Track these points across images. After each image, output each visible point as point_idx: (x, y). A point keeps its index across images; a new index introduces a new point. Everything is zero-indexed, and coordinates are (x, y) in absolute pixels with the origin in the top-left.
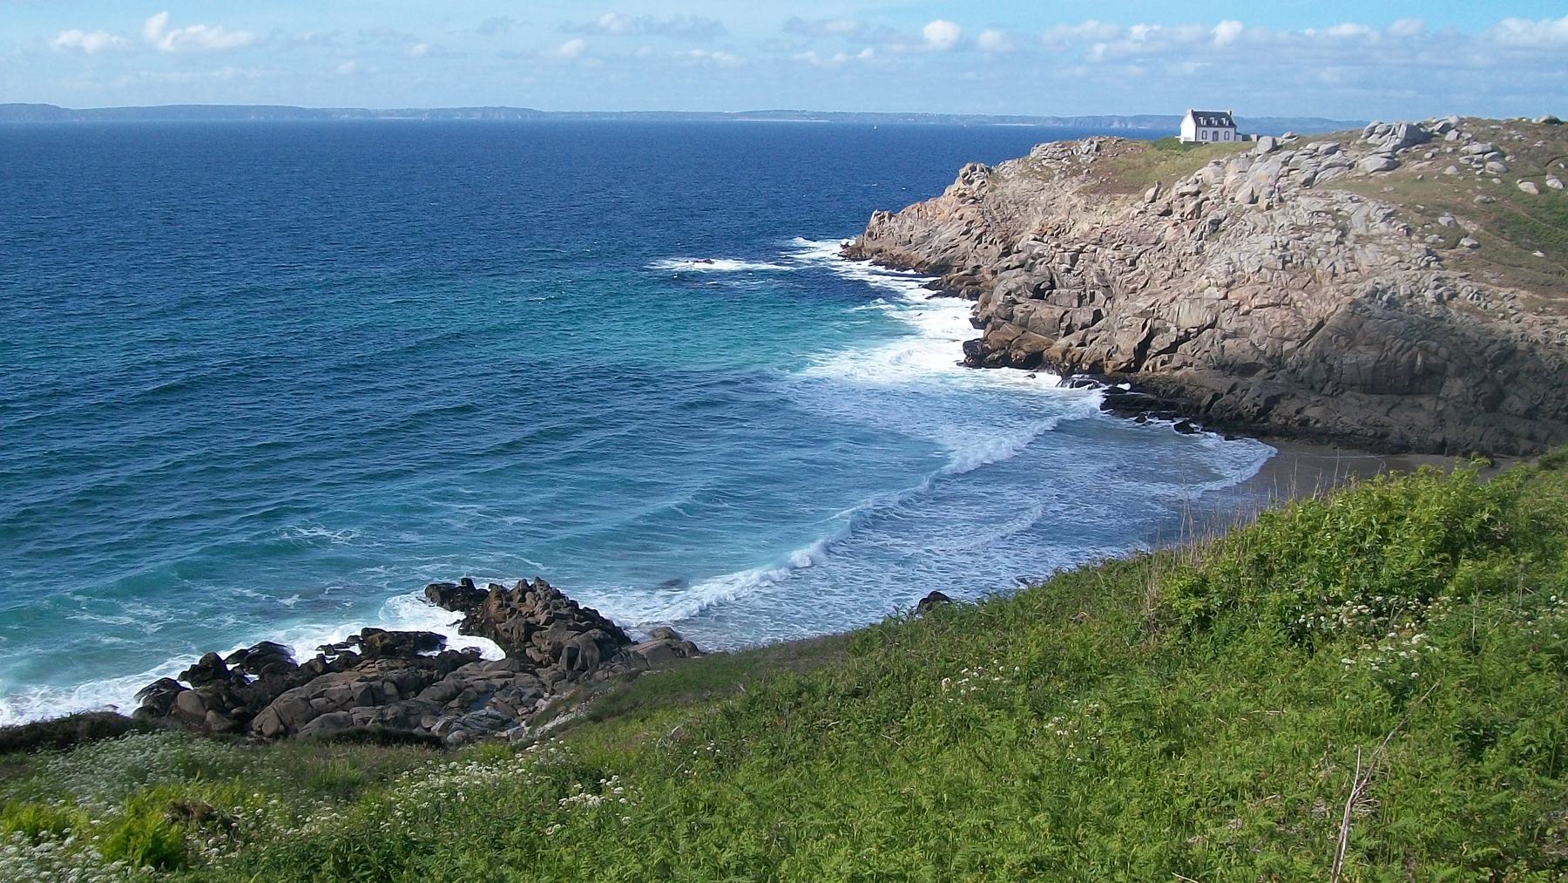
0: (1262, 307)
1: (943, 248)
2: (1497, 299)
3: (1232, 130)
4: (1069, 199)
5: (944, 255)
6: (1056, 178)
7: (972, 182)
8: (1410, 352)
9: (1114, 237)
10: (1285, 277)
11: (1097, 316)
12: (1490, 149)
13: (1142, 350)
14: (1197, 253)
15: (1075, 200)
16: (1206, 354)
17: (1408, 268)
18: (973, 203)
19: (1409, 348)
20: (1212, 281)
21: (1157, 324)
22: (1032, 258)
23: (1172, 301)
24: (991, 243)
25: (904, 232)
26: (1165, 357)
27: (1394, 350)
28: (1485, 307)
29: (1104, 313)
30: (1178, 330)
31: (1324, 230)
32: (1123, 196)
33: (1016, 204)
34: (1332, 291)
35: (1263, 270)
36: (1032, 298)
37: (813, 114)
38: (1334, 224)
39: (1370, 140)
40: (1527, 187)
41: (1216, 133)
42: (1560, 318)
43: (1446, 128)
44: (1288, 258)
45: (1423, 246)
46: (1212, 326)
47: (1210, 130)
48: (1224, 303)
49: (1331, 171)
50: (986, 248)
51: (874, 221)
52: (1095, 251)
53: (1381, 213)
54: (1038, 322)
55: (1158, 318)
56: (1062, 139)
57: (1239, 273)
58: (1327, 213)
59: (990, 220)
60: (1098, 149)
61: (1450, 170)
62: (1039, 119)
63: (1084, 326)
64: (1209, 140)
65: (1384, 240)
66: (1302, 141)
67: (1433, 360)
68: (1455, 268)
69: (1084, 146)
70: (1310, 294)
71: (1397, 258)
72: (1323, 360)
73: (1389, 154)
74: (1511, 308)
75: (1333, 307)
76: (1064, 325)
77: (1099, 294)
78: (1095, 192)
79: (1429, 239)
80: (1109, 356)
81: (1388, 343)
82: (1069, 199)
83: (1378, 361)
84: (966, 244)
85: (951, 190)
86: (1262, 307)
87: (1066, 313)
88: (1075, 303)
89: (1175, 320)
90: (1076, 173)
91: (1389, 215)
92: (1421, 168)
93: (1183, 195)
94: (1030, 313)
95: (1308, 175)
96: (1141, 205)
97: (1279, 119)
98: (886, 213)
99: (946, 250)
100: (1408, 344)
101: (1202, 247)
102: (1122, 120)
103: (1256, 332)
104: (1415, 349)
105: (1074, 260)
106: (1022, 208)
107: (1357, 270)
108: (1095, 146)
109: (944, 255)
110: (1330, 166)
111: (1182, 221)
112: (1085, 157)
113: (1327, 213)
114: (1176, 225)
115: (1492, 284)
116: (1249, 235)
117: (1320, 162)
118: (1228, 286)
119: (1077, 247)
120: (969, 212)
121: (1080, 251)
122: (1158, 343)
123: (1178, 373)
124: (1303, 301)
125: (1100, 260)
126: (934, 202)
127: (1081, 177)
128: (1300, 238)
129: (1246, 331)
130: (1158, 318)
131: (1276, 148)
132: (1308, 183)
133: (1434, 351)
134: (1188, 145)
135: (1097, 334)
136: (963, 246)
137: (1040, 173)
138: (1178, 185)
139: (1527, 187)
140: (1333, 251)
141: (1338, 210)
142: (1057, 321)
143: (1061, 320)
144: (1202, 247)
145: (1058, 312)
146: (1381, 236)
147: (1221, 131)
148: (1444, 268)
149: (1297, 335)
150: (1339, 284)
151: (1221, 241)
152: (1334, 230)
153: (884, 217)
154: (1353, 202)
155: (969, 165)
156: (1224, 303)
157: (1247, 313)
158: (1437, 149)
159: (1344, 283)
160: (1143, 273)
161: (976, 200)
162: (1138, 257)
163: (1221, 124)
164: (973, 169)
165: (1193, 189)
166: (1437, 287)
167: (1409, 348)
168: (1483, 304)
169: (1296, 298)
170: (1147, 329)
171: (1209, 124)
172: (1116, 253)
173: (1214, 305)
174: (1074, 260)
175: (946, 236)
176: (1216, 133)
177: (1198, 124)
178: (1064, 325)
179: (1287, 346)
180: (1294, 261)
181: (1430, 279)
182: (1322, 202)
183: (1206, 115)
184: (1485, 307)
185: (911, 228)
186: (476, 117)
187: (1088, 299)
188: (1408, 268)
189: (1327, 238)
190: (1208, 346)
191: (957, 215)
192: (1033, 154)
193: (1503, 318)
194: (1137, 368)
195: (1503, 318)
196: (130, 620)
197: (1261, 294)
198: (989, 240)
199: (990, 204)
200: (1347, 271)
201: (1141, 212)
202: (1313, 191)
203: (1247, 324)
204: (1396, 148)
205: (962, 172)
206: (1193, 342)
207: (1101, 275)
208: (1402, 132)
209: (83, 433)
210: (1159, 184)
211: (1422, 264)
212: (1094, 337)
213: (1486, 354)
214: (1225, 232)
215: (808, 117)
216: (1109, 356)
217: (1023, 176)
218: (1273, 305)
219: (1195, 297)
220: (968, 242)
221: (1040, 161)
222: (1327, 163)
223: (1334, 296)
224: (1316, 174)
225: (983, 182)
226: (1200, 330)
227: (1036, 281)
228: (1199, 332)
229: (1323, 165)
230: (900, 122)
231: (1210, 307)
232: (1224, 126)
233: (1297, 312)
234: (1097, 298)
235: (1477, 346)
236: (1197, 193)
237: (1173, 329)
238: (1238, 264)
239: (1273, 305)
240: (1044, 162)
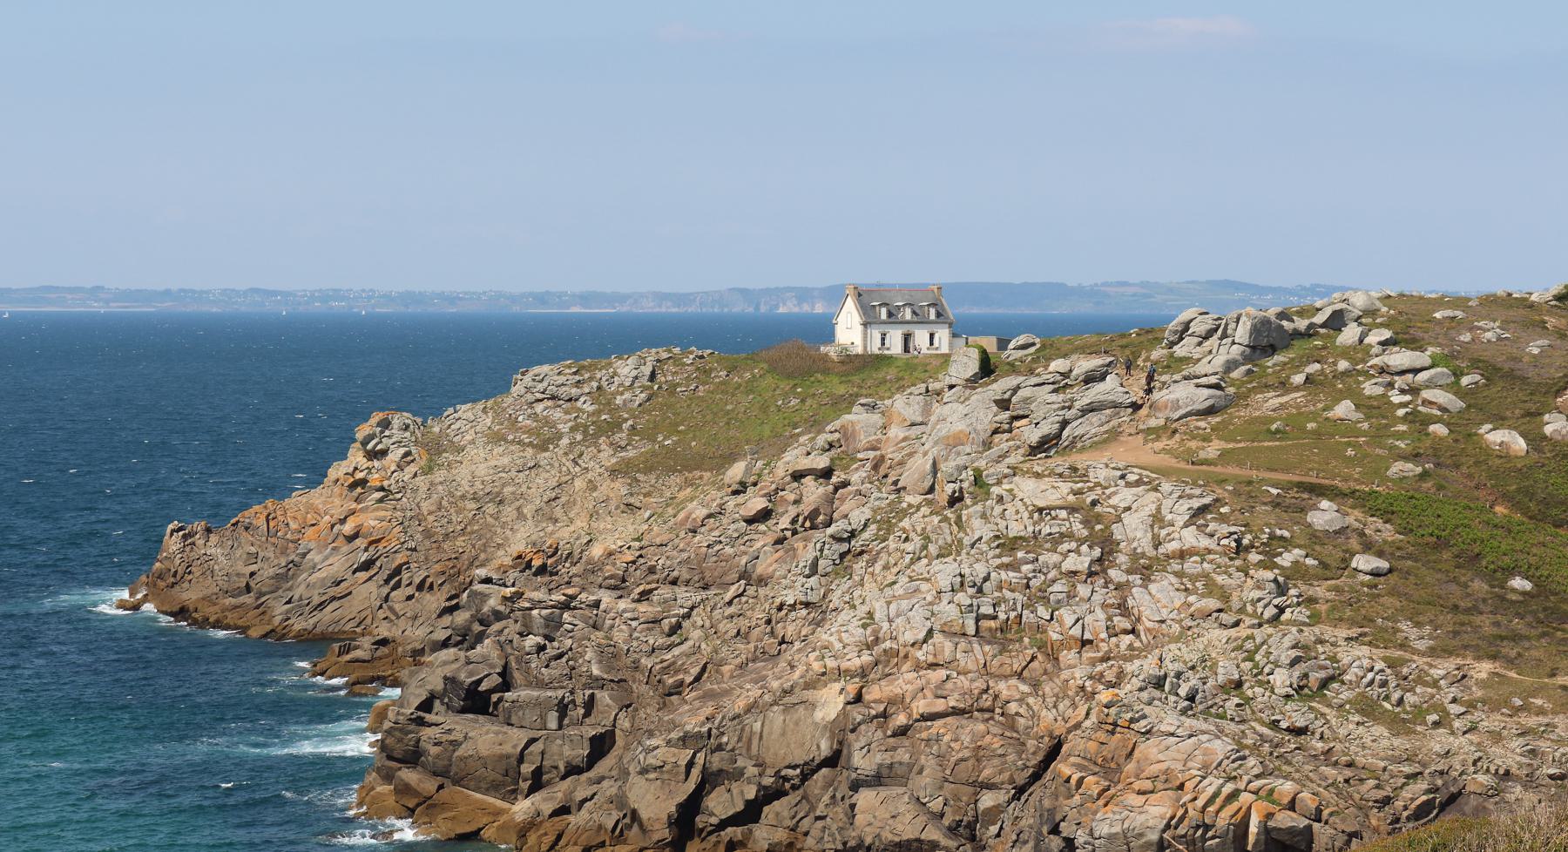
1: (316, 600)
2: (1426, 684)
5: (318, 616)
6: (565, 441)
8: (1235, 806)
9: (652, 570)
11: (601, 745)
12: (1428, 362)
16: (820, 824)
17: (1237, 624)
18: (381, 500)
19: (1233, 796)
21: (717, 761)
22: (481, 622)
27: (1200, 803)
28: (1400, 702)
31: (1065, 547)
34: (1079, 674)
35: (938, 638)
36: (463, 711)
38: (1085, 533)
39: (1179, 351)
40: (1507, 439)
42: (1559, 720)
43: (1337, 321)
45: (1269, 575)
46: (832, 761)
49: (1094, 418)
50: (410, 598)
51: (173, 544)
53: (1184, 506)
56: (576, 355)
58: (1072, 510)
59: (418, 537)
61: (1344, 409)
62: (622, 298)
63: (573, 770)
65: (1191, 566)
66: (1048, 351)
67: (1285, 820)
68: (1337, 622)
69: (625, 369)
70: (1036, 685)
71: (1213, 603)
72: (1055, 830)
73: (1213, 380)
74: (1454, 701)
75: (1082, 710)
76: (527, 769)
78: (648, 470)
79: (1286, 559)
81: (1189, 785)
83: (1168, 826)
85: (338, 471)
87: (532, 741)
88: (553, 723)
91: (1203, 510)
92: (1282, 406)
93: (798, 476)
94: (455, 744)
95: (1048, 428)
96: (715, 497)
97: (1144, 285)
98: (199, 526)
100: (1229, 788)
103: (920, 772)
104: (1246, 798)
107: (1133, 631)
108: (647, 370)
110: (1091, 409)
111: (795, 532)
113: (1072, 510)
114: (780, 541)
115: (1415, 652)
116: (912, 562)
117: (1072, 400)
118: (863, 673)
122: (720, 804)
124: (1021, 701)
125: (608, 622)
129: (899, 770)
130: (720, 748)
131: (987, 369)
132: (1044, 446)
133: (1286, 801)
135: (594, 788)
137: (529, 431)
138: (788, 456)
139: (1507, 439)
140: (1083, 590)
141: (1094, 503)
142: (514, 761)
145: (517, 737)
146: (1182, 555)
148: (1315, 619)
149: (1006, 775)
150: (1093, 663)
151: (857, 578)
152: (1084, 548)
154: (1128, 485)
155: (377, 417)
157: (903, 732)
158: (1317, 366)
159: (1106, 659)
160: (697, 650)
162: (688, 616)
164: (385, 424)
165: (822, 462)
166: (1294, 662)
167: (1233, 796)
168: (1396, 696)
169: (1005, 694)
172: (643, 607)
179: (987, 800)
180: (1002, 616)
181: (1282, 646)
182: (1065, 487)
184: (1400, 702)
188: (1237, 624)
189: (1071, 563)
190: (821, 806)
192: (517, 389)
193: (1436, 724)
195: (1436, 724)
200: (1113, 632)
201: (710, 516)
202: (1051, 463)
203: (903, 755)
204: (1230, 366)
205: (362, 431)
206: (792, 798)
207: (609, 655)
208: (1242, 333)
211: (1267, 615)
212: (589, 793)
213: (1399, 804)
214: (866, 557)
217: (497, 438)
218: (956, 712)
220: (372, 586)
222: (1086, 401)
223: (1083, 688)
224: (1064, 424)
225: (408, 454)
226: (808, 771)
227: (471, 674)
228: (805, 777)
229: (1078, 405)
233: (1010, 722)
234: (599, 706)
235: (1378, 787)
236: (826, 474)
238: (885, 625)
240: (539, 408)
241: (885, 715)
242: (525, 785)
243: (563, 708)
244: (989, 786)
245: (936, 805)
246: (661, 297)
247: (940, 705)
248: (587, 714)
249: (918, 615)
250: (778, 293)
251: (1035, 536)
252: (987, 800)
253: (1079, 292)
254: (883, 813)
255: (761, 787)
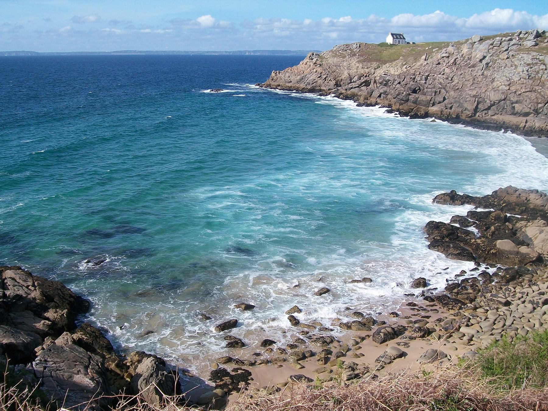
0: (526, 92)
3: (404, 40)
4: (355, 65)
5: (313, 85)
7: (312, 59)
10: (531, 82)
13: (476, 110)
14: (482, 75)
15: (357, 65)
20: (503, 83)
23: (486, 91)
24: (330, 80)
25: (286, 78)
26: (486, 111)
29: (446, 97)
30: (491, 101)
32: (375, 63)
33: (335, 66)
37: (139, 52)
41: (399, 41)
44: (530, 75)
46: (504, 100)
47: (397, 40)
48: (509, 91)
51: (273, 74)
52: (434, 76)
54: (421, 101)
55: (480, 98)
57: (512, 80)
60: (360, 47)
62: (220, 52)
64: (397, 43)
76: (432, 102)
77: (443, 91)
78: (364, 62)
80: (462, 112)
82: (355, 65)
84: (320, 81)
86: (526, 92)
88: (433, 94)
89: (488, 98)
90: (355, 55)
93: (443, 57)
99: (313, 83)
101: (483, 72)
102: (249, 52)
105: (426, 79)
106: (339, 68)
109: (313, 85)
112: (356, 50)
118: (509, 85)
119: (427, 74)
120: (319, 70)
121: (428, 76)
123: (493, 117)
126: (296, 67)
127: (357, 57)
128: (531, 68)
129: (521, 101)
130: (480, 98)
134: (391, 45)
136: (319, 82)
143: (430, 101)
144: (483, 72)
147: (401, 40)
153: (276, 73)
156: (509, 91)
157: (520, 94)
161: (320, 65)
163: (401, 38)
170: (476, 102)
171: (397, 38)
173: (505, 92)
174: (426, 79)
175: (312, 78)
176: (399, 41)
177: (394, 38)
178: (432, 102)
179: (540, 105)
180: (532, 76)
183: (396, 35)
185: (289, 77)
186: (14, 55)
187: (438, 93)
191: (315, 71)
194: (475, 115)
196: (223, 220)
197: (524, 88)
198: (329, 79)
199: (326, 66)
203: (521, 98)
209: (297, 137)
210: (426, 54)
215: (137, 53)
216: (462, 112)
218: (530, 91)
219: (495, 90)
221: (339, 51)
226: (500, 101)
228: (499, 102)
230: (171, 54)
231: (503, 93)
232: (401, 39)
237: (488, 101)
239: (530, 91)
240: (340, 51)
241: (515, 92)
242: (431, 105)
243: (436, 92)
244: (540, 103)
245: (530, 106)
246: (226, 52)
247: (527, 90)
248: (439, 94)
249: (518, 76)
250: (245, 51)
251: (532, 63)
252: (540, 105)
253: (293, 52)
254: (521, 108)
255: (491, 104)
